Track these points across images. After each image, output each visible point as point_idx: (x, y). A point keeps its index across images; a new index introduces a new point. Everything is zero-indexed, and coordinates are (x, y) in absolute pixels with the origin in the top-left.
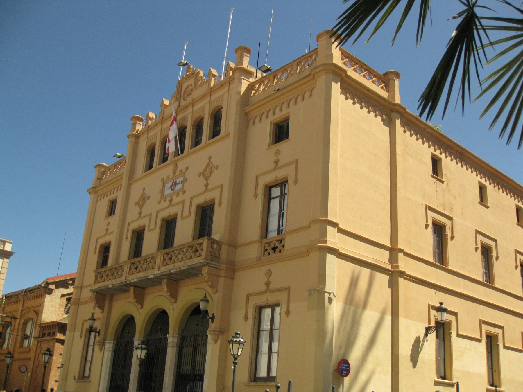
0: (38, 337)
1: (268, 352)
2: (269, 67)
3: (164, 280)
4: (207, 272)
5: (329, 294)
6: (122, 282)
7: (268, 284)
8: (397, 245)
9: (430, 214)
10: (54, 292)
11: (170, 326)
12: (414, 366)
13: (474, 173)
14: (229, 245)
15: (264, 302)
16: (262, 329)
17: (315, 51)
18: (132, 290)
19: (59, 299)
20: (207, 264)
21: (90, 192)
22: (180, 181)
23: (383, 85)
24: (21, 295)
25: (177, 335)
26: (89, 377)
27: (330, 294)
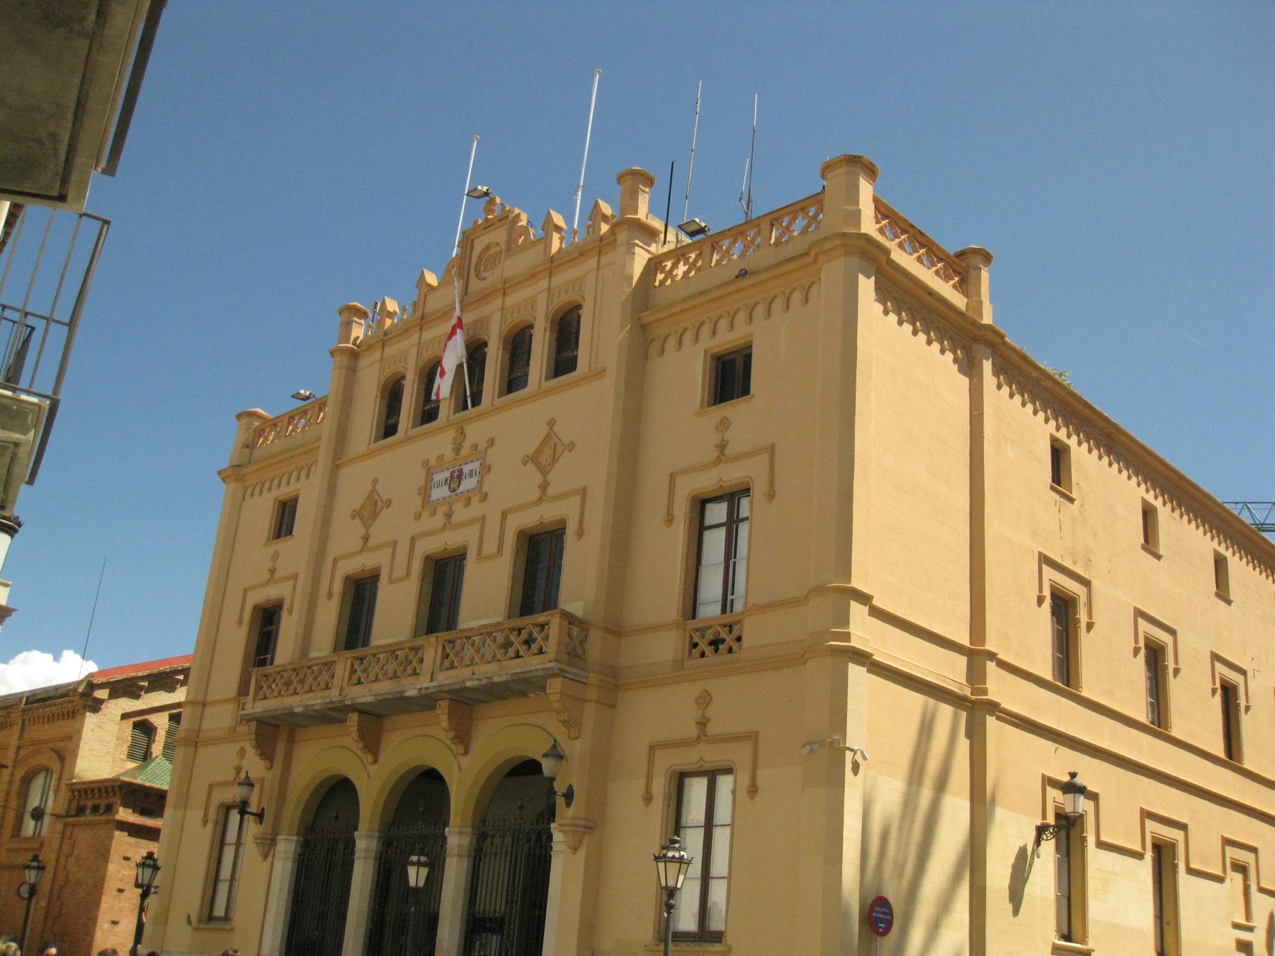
0: (64, 814)
1: (700, 876)
2: (703, 225)
3: (442, 703)
4: (559, 690)
5: (853, 753)
6: (331, 702)
7: (702, 724)
8: (983, 644)
9: (1048, 572)
10: (106, 707)
11: (452, 807)
12: (1016, 912)
13: (1134, 479)
14: (607, 630)
15: (692, 764)
16: (684, 822)
17: (817, 199)
18: (354, 722)
19: (117, 724)
20: (561, 673)
21: (226, 477)
22: (471, 471)
23: (957, 279)
24: (16, 710)
25: (469, 830)
26: (227, 918)
27: (854, 752)
